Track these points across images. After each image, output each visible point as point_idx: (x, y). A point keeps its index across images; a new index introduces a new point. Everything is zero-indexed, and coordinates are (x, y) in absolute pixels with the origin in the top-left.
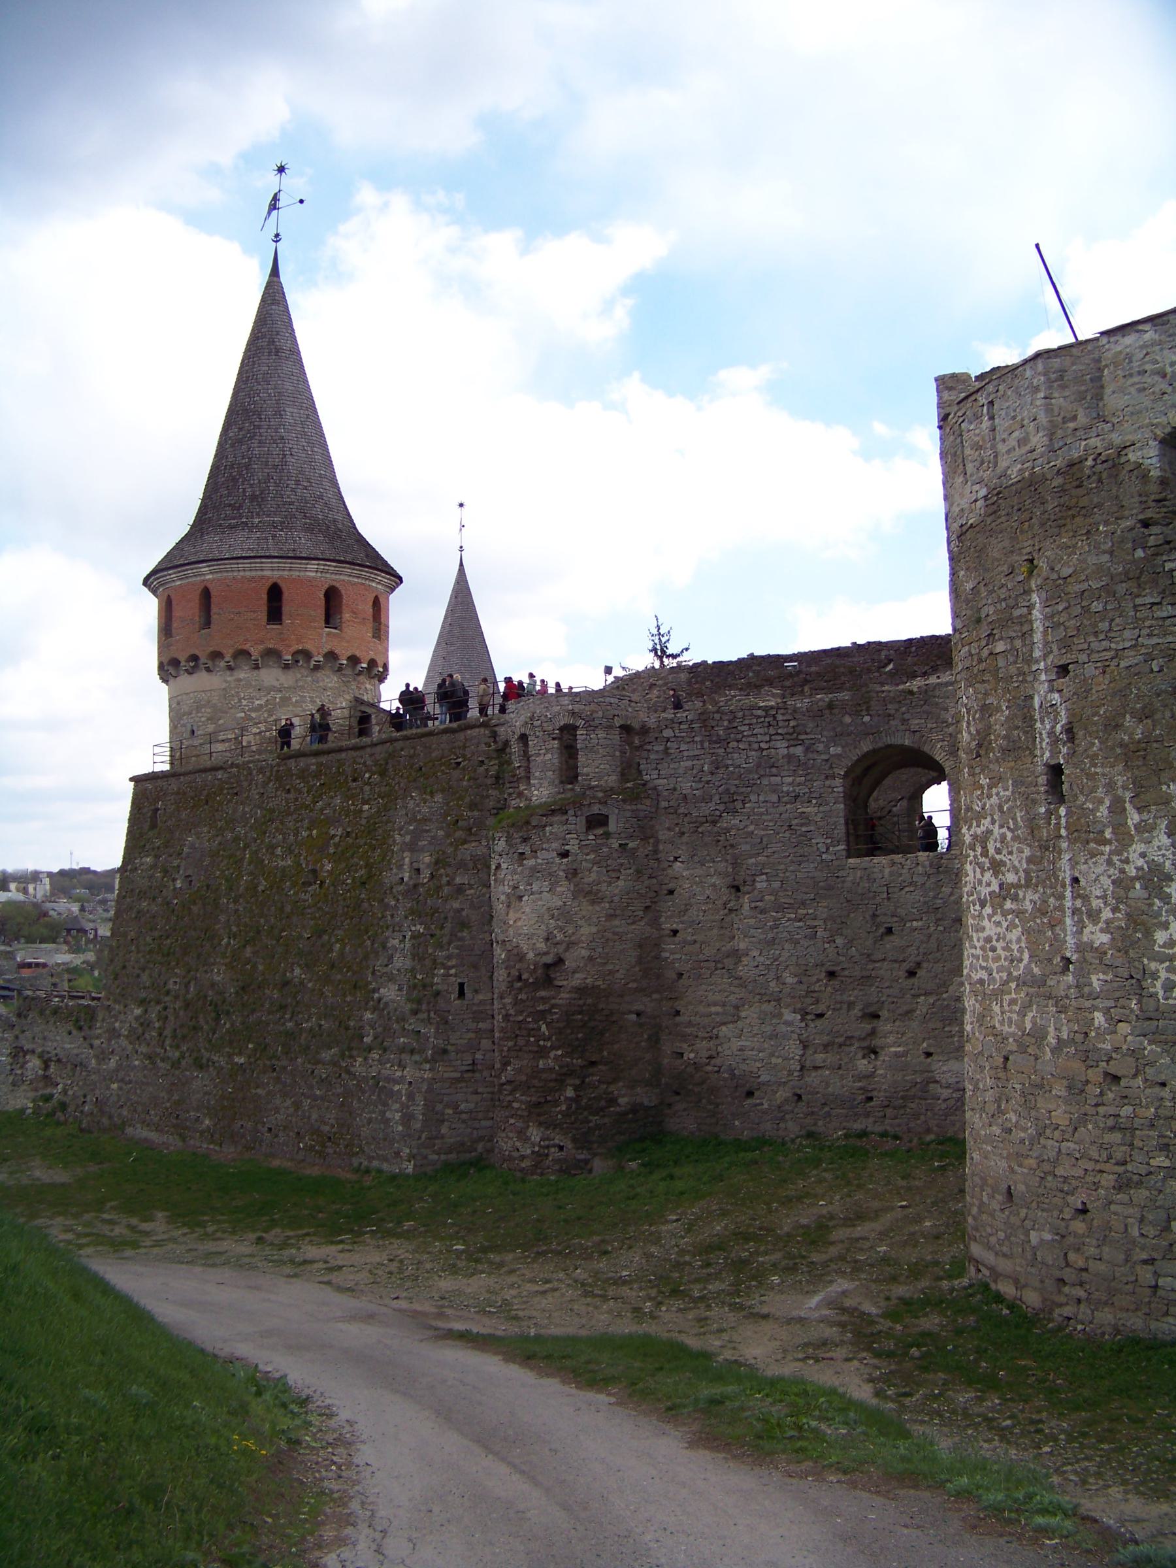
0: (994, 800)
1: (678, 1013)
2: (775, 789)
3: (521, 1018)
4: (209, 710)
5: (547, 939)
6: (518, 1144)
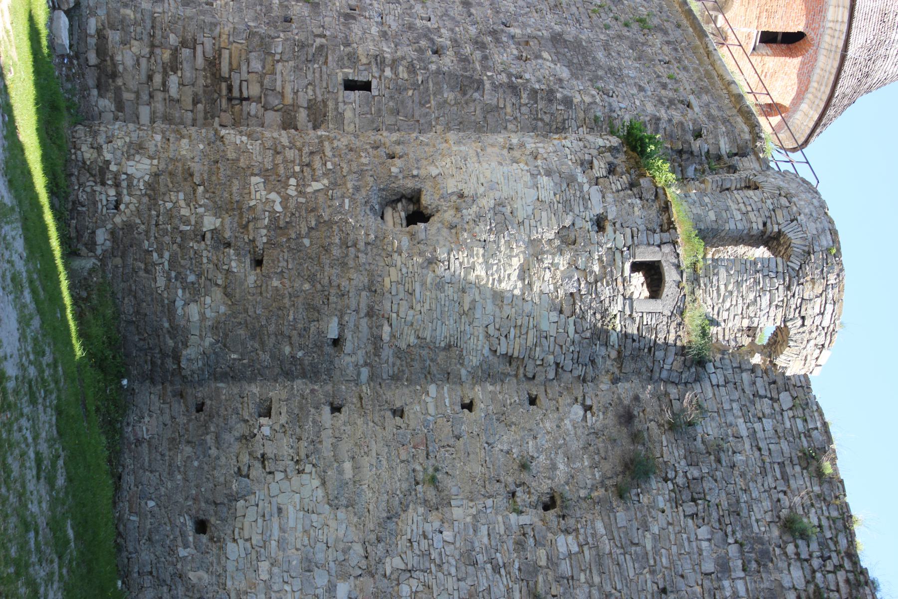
1: (336, 409)
2: (724, 567)
5: (461, 196)
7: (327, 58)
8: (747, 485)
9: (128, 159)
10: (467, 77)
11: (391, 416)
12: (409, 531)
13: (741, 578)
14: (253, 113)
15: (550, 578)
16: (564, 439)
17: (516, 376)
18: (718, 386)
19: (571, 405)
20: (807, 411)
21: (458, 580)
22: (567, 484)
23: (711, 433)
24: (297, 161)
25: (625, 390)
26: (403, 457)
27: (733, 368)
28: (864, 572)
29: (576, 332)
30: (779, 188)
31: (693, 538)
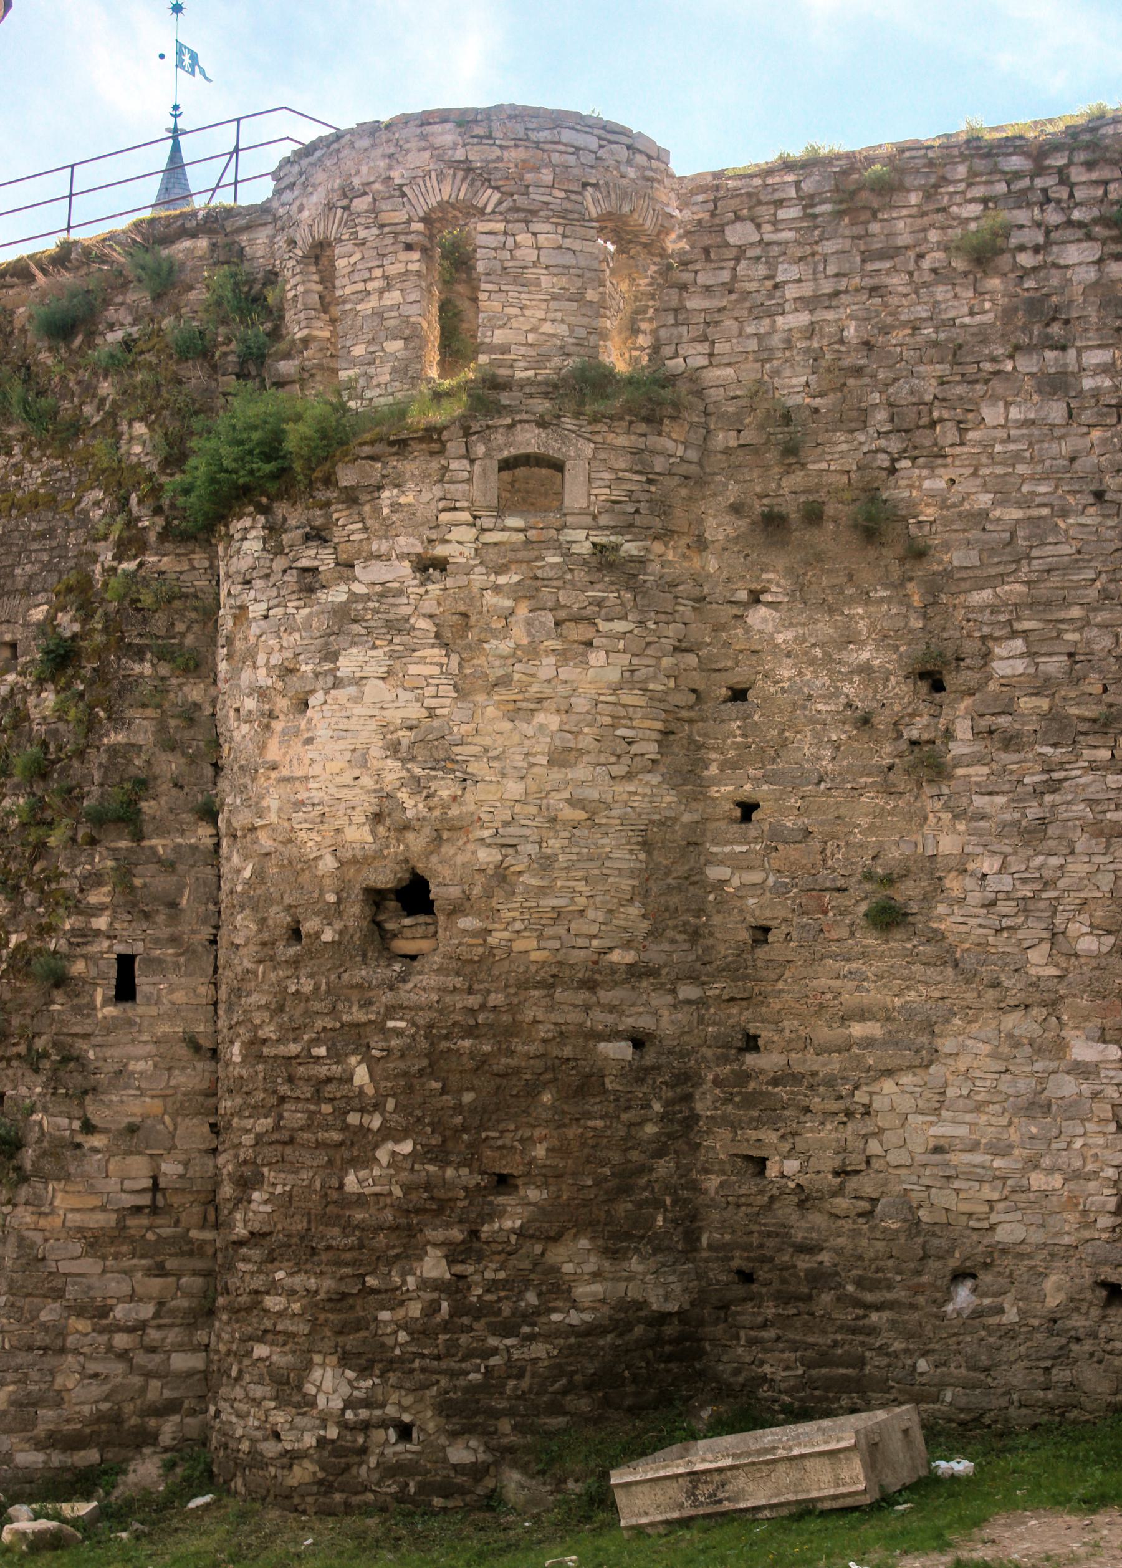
1: (751, 1043)
2: (1056, 384)
3: (294, 1048)
5: (377, 818)
6: (279, 1418)
7: (76, 1035)
8: (904, 325)
9: (313, 1404)
10: (105, 776)
11: (766, 948)
12: (981, 931)
13: (1079, 355)
14: (180, 1169)
15: (1072, 695)
16: (814, 645)
17: (691, 721)
18: (711, 355)
19: (748, 630)
20: (763, 198)
21: (1072, 853)
22: (897, 647)
23: (803, 379)
24: (312, 1107)
25: (719, 528)
26: (845, 934)
27: (676, 324)
28: (1073, 132)
29: (624, 618)
30: (330, 207)
31: (1002, 434)
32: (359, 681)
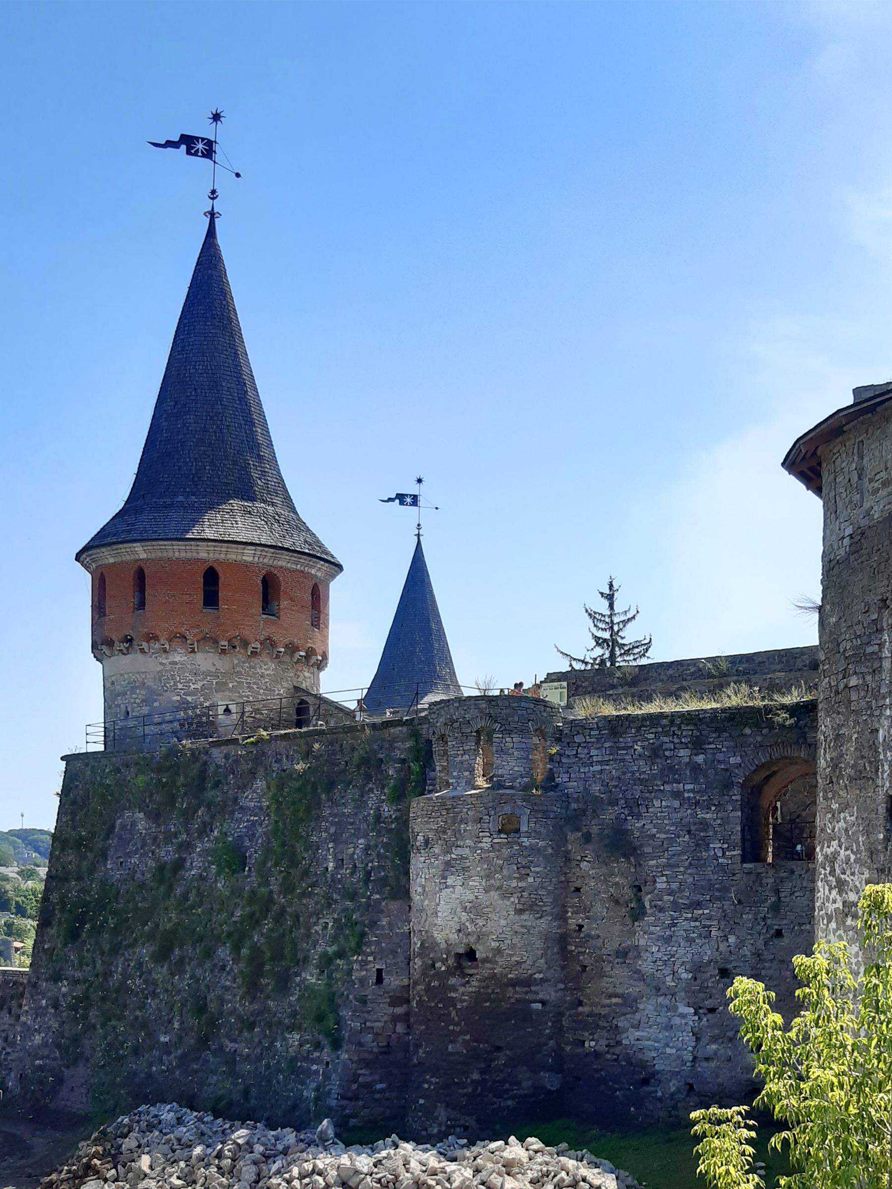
0: (842, 824)
1: (580, 1003)
2: (677, 795)
4: (144, 692)
5: (460, 931)
8: (630, 772)
30: (446, 724)
32: (453, 887)
